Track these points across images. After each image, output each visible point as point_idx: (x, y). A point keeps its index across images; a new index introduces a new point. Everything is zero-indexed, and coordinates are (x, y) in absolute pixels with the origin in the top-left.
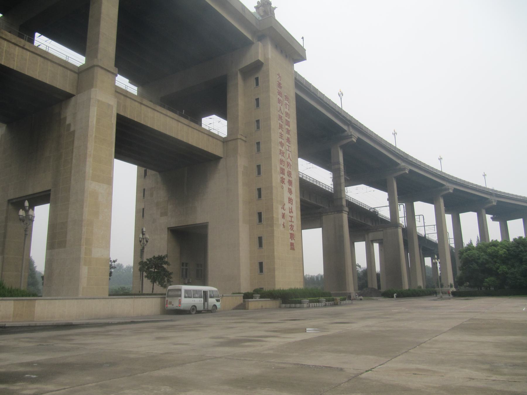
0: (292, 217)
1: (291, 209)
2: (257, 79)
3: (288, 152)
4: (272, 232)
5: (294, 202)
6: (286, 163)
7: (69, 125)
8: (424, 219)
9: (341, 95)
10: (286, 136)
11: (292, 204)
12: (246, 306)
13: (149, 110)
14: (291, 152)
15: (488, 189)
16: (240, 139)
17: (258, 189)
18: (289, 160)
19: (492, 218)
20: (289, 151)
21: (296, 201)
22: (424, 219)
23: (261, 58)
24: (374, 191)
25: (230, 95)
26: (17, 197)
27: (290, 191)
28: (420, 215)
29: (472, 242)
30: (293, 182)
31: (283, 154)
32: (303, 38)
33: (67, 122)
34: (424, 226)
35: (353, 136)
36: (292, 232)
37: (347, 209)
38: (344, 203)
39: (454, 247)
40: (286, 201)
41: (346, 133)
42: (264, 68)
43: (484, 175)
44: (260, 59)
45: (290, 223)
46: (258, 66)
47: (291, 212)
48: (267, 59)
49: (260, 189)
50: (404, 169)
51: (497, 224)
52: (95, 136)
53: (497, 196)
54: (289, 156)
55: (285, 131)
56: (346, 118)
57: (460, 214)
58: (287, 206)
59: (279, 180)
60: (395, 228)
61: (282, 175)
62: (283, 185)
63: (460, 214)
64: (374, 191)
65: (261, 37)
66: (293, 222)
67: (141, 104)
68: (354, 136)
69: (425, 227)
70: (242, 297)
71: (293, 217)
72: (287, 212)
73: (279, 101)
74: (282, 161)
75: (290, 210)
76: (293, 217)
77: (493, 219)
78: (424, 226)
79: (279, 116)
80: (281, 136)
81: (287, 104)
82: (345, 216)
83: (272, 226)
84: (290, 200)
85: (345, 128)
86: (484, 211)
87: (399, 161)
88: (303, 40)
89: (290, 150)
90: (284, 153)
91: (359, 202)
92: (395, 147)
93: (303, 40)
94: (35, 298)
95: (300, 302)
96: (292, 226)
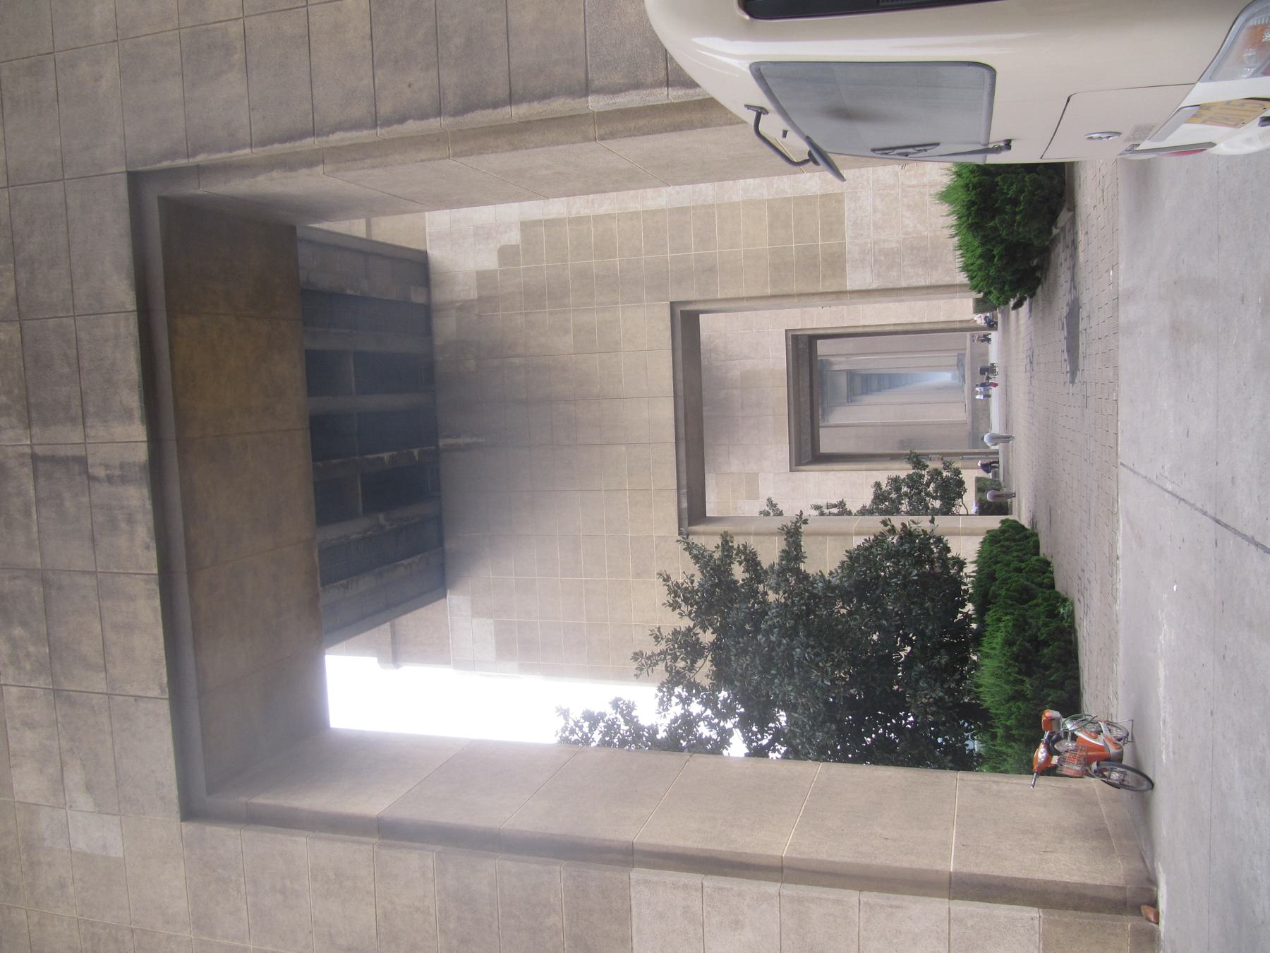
7: (507, 254)
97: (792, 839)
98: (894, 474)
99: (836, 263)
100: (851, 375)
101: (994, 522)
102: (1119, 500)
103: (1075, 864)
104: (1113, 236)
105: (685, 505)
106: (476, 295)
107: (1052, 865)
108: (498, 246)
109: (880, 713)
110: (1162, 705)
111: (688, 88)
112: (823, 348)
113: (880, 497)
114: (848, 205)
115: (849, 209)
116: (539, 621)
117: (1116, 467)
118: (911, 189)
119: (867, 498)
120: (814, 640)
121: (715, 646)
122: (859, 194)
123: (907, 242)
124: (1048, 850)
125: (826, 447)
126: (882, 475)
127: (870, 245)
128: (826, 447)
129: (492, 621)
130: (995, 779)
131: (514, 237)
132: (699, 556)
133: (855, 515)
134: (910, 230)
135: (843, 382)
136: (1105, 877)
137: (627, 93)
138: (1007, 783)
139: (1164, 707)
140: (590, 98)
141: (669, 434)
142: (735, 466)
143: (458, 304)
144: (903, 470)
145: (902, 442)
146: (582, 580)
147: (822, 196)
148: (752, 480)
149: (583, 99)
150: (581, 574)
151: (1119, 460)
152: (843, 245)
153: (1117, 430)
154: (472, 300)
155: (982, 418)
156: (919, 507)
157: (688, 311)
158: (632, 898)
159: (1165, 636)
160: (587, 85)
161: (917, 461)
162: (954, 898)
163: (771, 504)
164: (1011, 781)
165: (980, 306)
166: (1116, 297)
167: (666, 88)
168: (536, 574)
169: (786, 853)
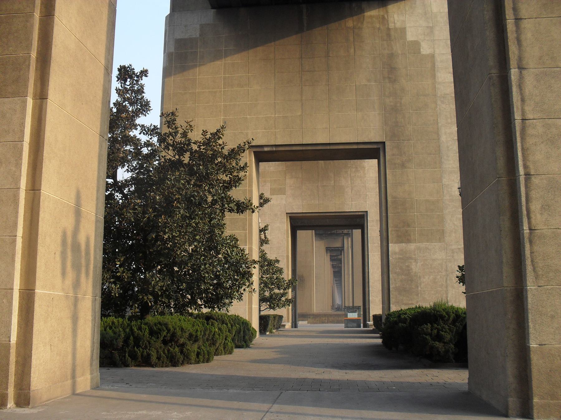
7: (416, 45)
33: (410, 36)
97: (53, 197)
98: (285, 271)
99: (405, 238)
100: (340, 250)
101: (255, 324)
102: (260, 391)
103: (44, 362)
104: (200, 385)
105: (266, 149)
106: (391, 27)
107: (42, 349)
108: (420, 41)
109: (215, 293)
110: (136, 413)
111: (521, 132)
112: (357, 233)
113: (270, 263)
114: (437, 245)
115: (435, 246)
116: (222, 104)
117: (280, 390)
118: (445, 280)
119: (271, 256)
120: (241, 267)
121: (180, 162)
122: (443, 251)
123: (415, 278)
124: (52, 347)
125: (300, 233)
126: (285, 265)
127: (414, 257)
128: (300, 233)
129: (198, 36)
130: (97, 319)
131: (425, 49)
132: (235, 153)
133: (260, 248)
134: (422, 280)
135: (338, 244)
136: (36, 379)
137: (519, 94)
138: (95, 325)
139: (134, 414)
140: (517, 70)
141: (308, 140)
142: (290, 181)
143: (386, 17)
144: (287, 275)
145: (302, 277)
146: (221, 89)
147: (443, 231)
148: (281, 191)
149: (517, 66)
150: (225, 88)
151: (284, 391)
152: (415, 241)
153: (302, 391)
154: (388, 25)
155: (315, 320)
156: (264, 284)
157: (380, 152)
158: (14, 98)
159: (177, 415)
160: (523, 68)
161: (292, 284)
162: (20, 292)
163: (267, 201)
164: (95, 328)
165: (377, 318)
166: (380, 390)
167: (521, 119)
168: (362, 325)
169: (43, 193)
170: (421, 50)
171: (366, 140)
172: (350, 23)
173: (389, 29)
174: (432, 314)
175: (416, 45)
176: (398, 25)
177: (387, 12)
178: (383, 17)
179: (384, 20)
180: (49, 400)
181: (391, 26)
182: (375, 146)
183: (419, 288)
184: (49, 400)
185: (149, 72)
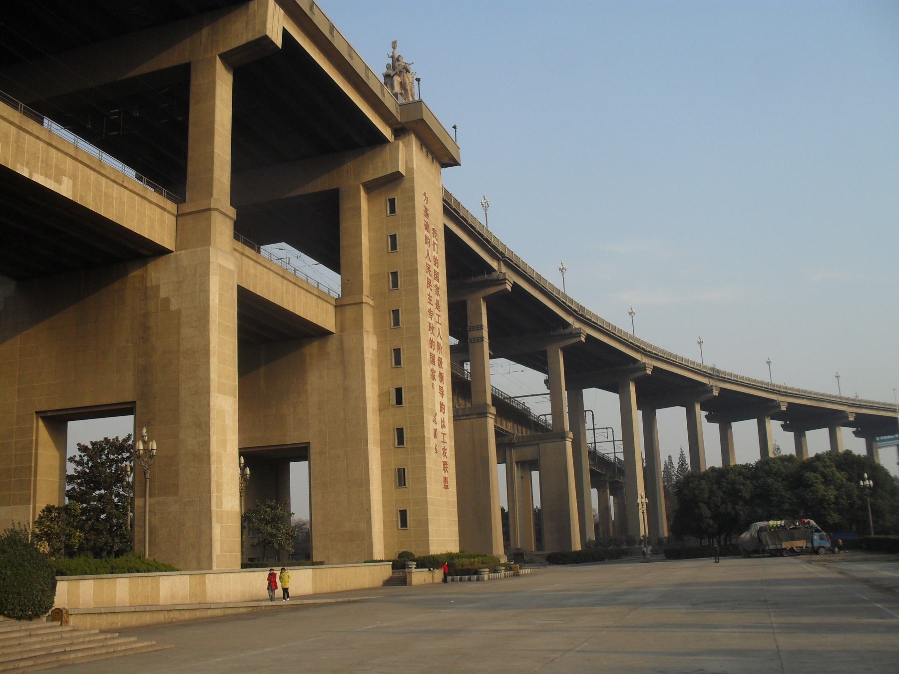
0: (444, 434)
1: (444, 422)
2: (392, 202)
3: (438, 326)
4: (423, 461)
5: (446, 409)
6: (436, 344)
7: (167, 300)
8: (593, 418)
9: (485, 206)
10: (435, 298)
11: (444, 413)
12: (408, 580)
13: (251, 262)
14: (440, 324)
15: (706, 367)
16: (366, 303)
17: (396, 389)
18: (439, 340)
19: (706, 416)
20: (438, 323)
21: (448, 407)
22: (593, 418)
23: (402, 169)
24: (523, 371)
25: (345, 224)
26: (57, 408)
27: (442, 394)
28: (588, 411)
29: (673, 460)
30: (445, 375)
31: (433, 331)
32: (455, 127)
33: (163, 294)
34: (594, 429)
35: (507, 281)
36: (445, 459)
37: (493, 410)
38: (489, 401)
39: (623, 460)
40: (438, 408)
41: (494, 275)
42: (406, 184)
43: (700, 343)
44: (400, 170)
45: (442, 445)
46: (395, 178)
47: (443, 426)
48: (410, 170)
49: (401, 389)
50: (578, 334)
51: (715, 427)
52: (219, 321)
53: (714, 378)
54: (439, 333)
55: (434, 289)
56: (498, 249)
57: (656, 410)
58: (440, 416)
59: (429, 373)
60: (560, 440)
61: (432, 366)
62: (434, 382)
63: (656, 410)
64: (523, 371)
65: (400, 131)
66: (446, 443)
67: (243, 254)
68: (508, 280)
69: (595, 430)
70: (391, 566)
71: (445, 434)
72: (439, 427)
73: (427, 240)
74: (431, 342)
75: (443, 424)
76: (445, 434)
77: (710, 419)
78: (594, 429)
79: (435, 272)
80: (429, 299)
81: (435, 243)
82: (491, 422)
83: (422, 450)
84: (442, 405)
85: (494, 264)
86: (698, 407)
87: (570, 320)
88: (456, 131)
89: (440, 323)
90: (433, 328)
91: (504, 393)
92: (633, 337)
93: (456, 131)
94: (158, 573)
95: (476, 572)
96: (444, 449)
143: (145, 275)
154: (146, 284)
170: (171, 306)
171: (122, 401)
172: (116, 285)
173: (146, 288)
174: (871, 491)
175: (167, 300)
176: (154, 282)
177: (146, 270)
178: (143, 276)
179: (143, 279)
180: (723, 612)
181: (149, 284)
182: (129, 406)
183: (157, 540)
184: (723, 612)
185: (452, 126)
